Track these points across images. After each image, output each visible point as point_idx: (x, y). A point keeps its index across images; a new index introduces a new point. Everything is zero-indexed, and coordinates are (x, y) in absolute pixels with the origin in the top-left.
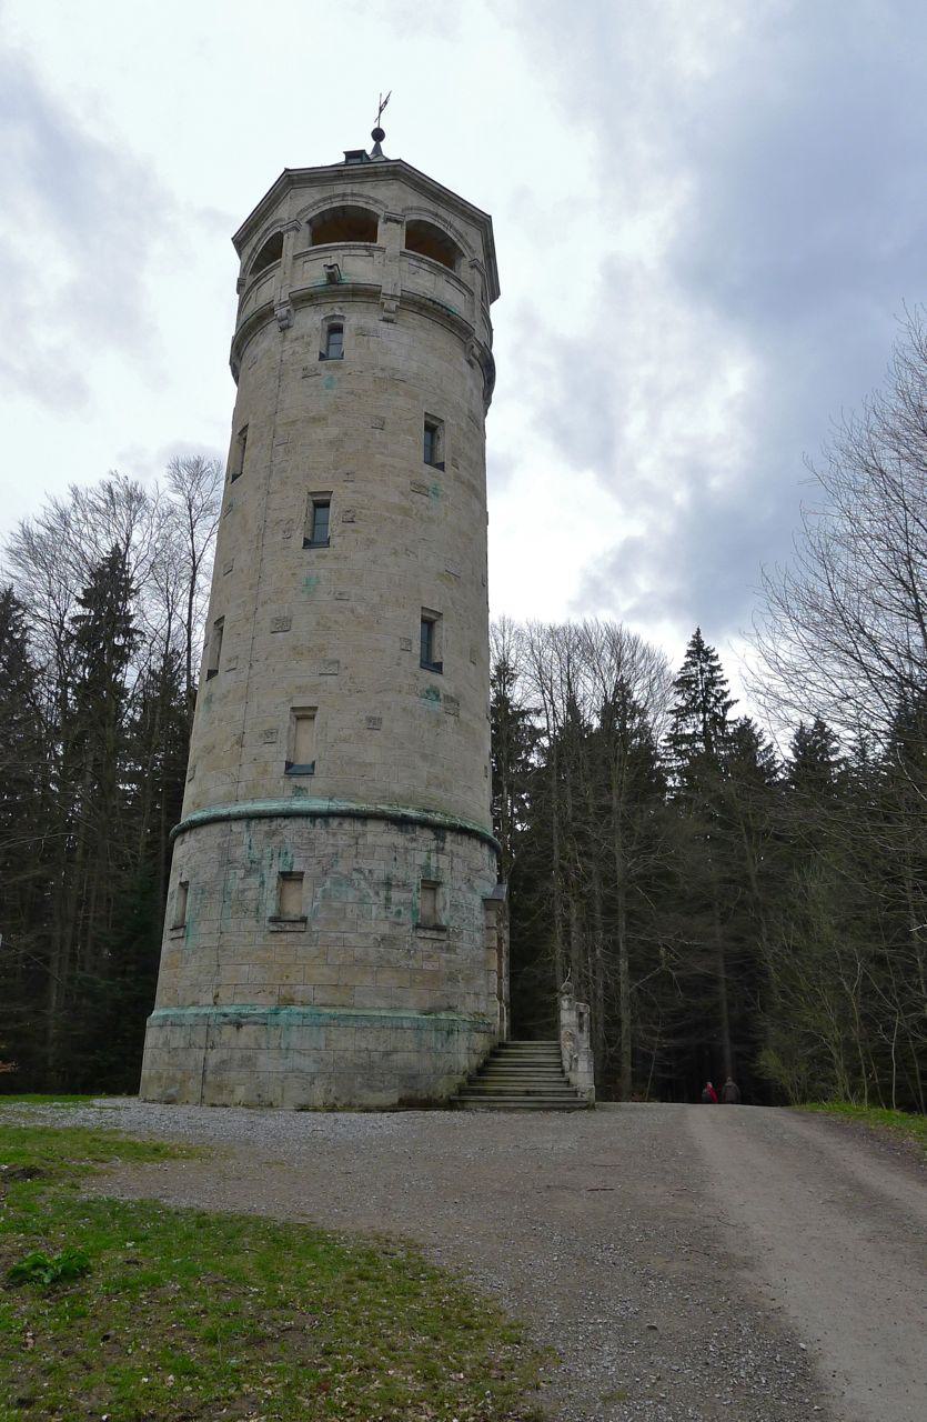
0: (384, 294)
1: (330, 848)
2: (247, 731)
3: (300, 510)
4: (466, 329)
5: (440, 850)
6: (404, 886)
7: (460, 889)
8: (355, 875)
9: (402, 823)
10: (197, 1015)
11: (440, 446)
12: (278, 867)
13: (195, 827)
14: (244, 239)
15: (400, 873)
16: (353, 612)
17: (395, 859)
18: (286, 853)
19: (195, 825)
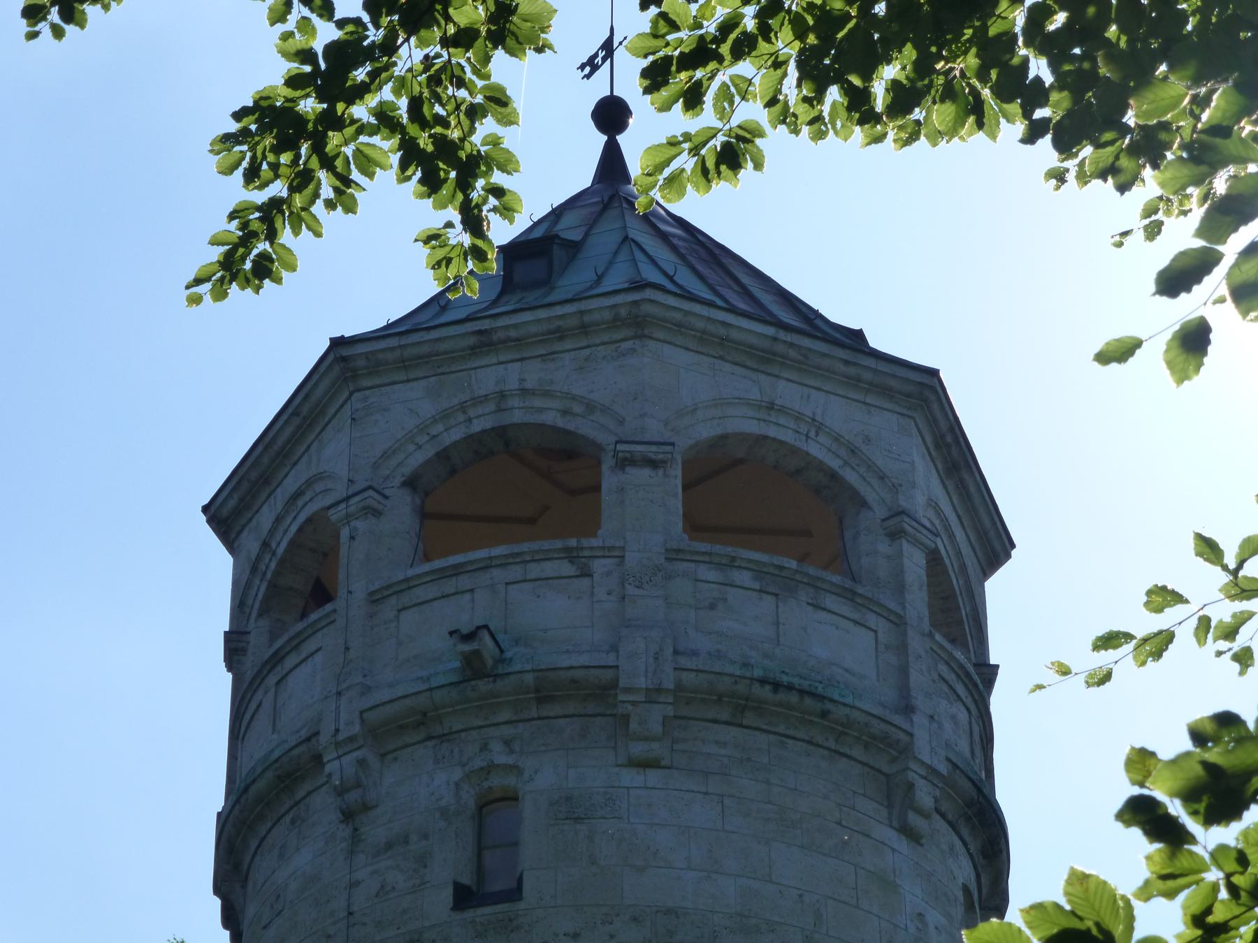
0: (627, 690)
14: (237, 512)
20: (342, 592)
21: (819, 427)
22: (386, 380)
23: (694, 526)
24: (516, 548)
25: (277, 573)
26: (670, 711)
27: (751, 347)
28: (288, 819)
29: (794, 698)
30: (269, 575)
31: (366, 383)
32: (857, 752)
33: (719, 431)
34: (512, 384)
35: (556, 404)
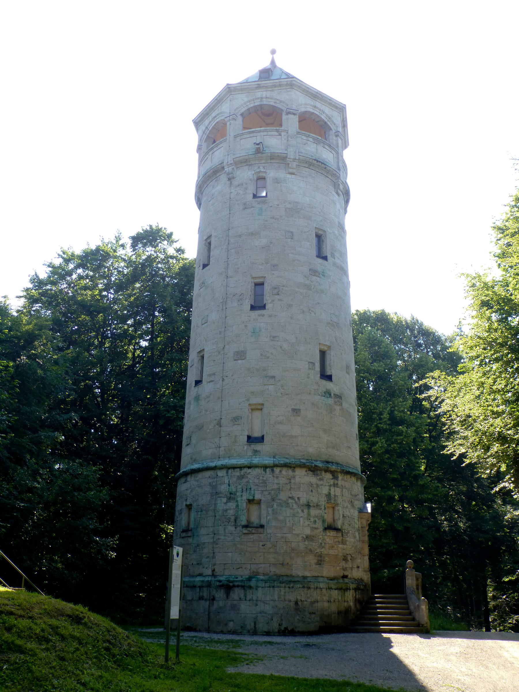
0: (289, 158)
1: (275, 485)
2: (223, 417)
3: (247, 289)
4: (335, 174)
5: (335, 485)
6: (317, 506)
7: (347, 507)
8: (290, 501)
9: (314, 469)
10: (203, 581)
11: (324, 246)
12: (246, 496)
13: (194, 473)
15: (314, 499)
16: (281, 347)
17: (312, 491)
18: (250, 489)
19: (186, 474)
20: (228, 135)
21: (324, 112)
22: (237, 93)
23: (300, 128)
24: (266, 128)
25: (209, 133)
26: (297, 163)
27: (313, 94)
28: (214, 180)
29: (320, 164)
30: (207, 134)
31: (233, 93)
32: (330, 177)
33: (305, 110)
34: (264, 96)
35: (273, 101)
